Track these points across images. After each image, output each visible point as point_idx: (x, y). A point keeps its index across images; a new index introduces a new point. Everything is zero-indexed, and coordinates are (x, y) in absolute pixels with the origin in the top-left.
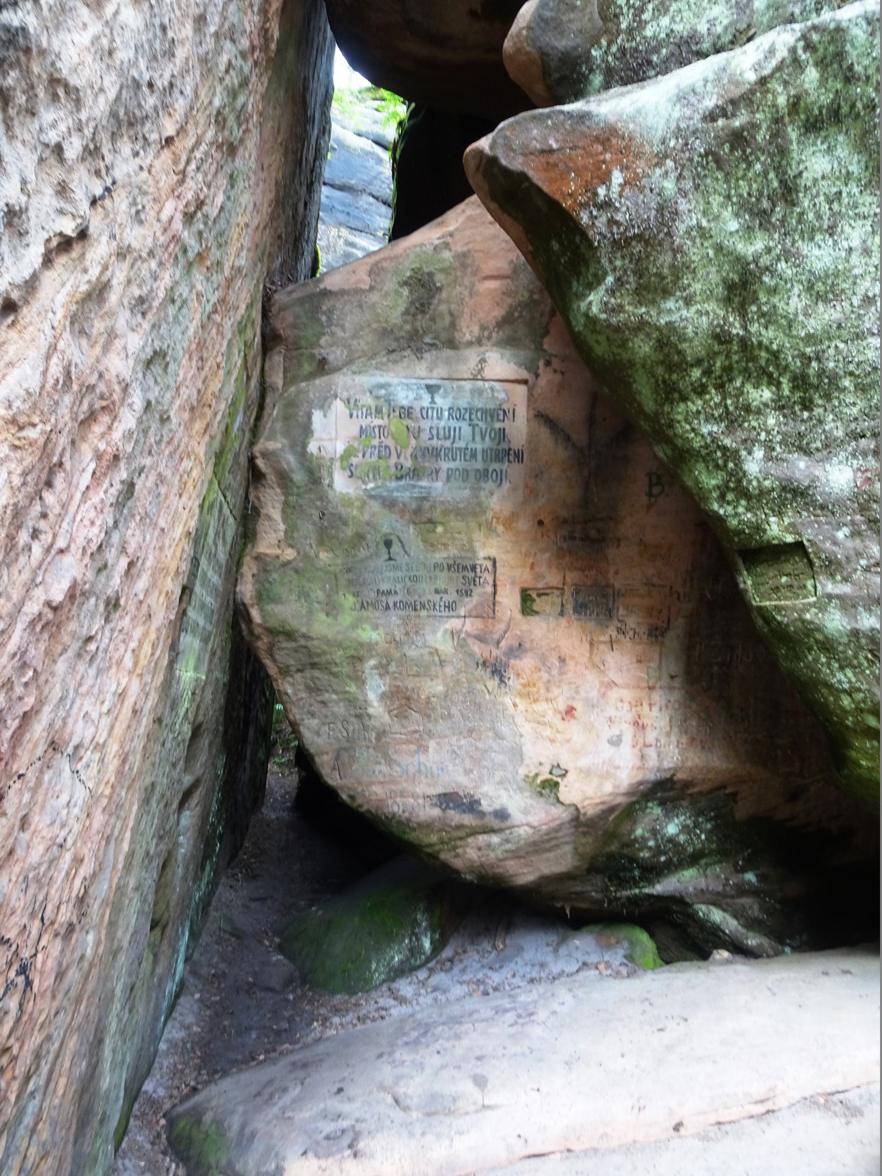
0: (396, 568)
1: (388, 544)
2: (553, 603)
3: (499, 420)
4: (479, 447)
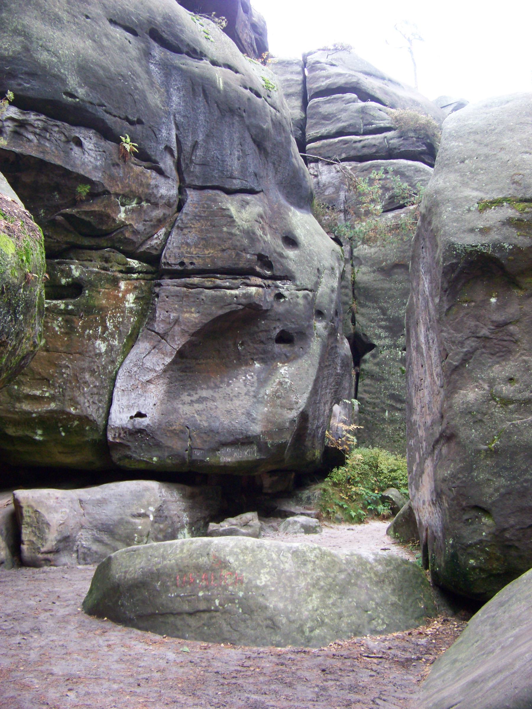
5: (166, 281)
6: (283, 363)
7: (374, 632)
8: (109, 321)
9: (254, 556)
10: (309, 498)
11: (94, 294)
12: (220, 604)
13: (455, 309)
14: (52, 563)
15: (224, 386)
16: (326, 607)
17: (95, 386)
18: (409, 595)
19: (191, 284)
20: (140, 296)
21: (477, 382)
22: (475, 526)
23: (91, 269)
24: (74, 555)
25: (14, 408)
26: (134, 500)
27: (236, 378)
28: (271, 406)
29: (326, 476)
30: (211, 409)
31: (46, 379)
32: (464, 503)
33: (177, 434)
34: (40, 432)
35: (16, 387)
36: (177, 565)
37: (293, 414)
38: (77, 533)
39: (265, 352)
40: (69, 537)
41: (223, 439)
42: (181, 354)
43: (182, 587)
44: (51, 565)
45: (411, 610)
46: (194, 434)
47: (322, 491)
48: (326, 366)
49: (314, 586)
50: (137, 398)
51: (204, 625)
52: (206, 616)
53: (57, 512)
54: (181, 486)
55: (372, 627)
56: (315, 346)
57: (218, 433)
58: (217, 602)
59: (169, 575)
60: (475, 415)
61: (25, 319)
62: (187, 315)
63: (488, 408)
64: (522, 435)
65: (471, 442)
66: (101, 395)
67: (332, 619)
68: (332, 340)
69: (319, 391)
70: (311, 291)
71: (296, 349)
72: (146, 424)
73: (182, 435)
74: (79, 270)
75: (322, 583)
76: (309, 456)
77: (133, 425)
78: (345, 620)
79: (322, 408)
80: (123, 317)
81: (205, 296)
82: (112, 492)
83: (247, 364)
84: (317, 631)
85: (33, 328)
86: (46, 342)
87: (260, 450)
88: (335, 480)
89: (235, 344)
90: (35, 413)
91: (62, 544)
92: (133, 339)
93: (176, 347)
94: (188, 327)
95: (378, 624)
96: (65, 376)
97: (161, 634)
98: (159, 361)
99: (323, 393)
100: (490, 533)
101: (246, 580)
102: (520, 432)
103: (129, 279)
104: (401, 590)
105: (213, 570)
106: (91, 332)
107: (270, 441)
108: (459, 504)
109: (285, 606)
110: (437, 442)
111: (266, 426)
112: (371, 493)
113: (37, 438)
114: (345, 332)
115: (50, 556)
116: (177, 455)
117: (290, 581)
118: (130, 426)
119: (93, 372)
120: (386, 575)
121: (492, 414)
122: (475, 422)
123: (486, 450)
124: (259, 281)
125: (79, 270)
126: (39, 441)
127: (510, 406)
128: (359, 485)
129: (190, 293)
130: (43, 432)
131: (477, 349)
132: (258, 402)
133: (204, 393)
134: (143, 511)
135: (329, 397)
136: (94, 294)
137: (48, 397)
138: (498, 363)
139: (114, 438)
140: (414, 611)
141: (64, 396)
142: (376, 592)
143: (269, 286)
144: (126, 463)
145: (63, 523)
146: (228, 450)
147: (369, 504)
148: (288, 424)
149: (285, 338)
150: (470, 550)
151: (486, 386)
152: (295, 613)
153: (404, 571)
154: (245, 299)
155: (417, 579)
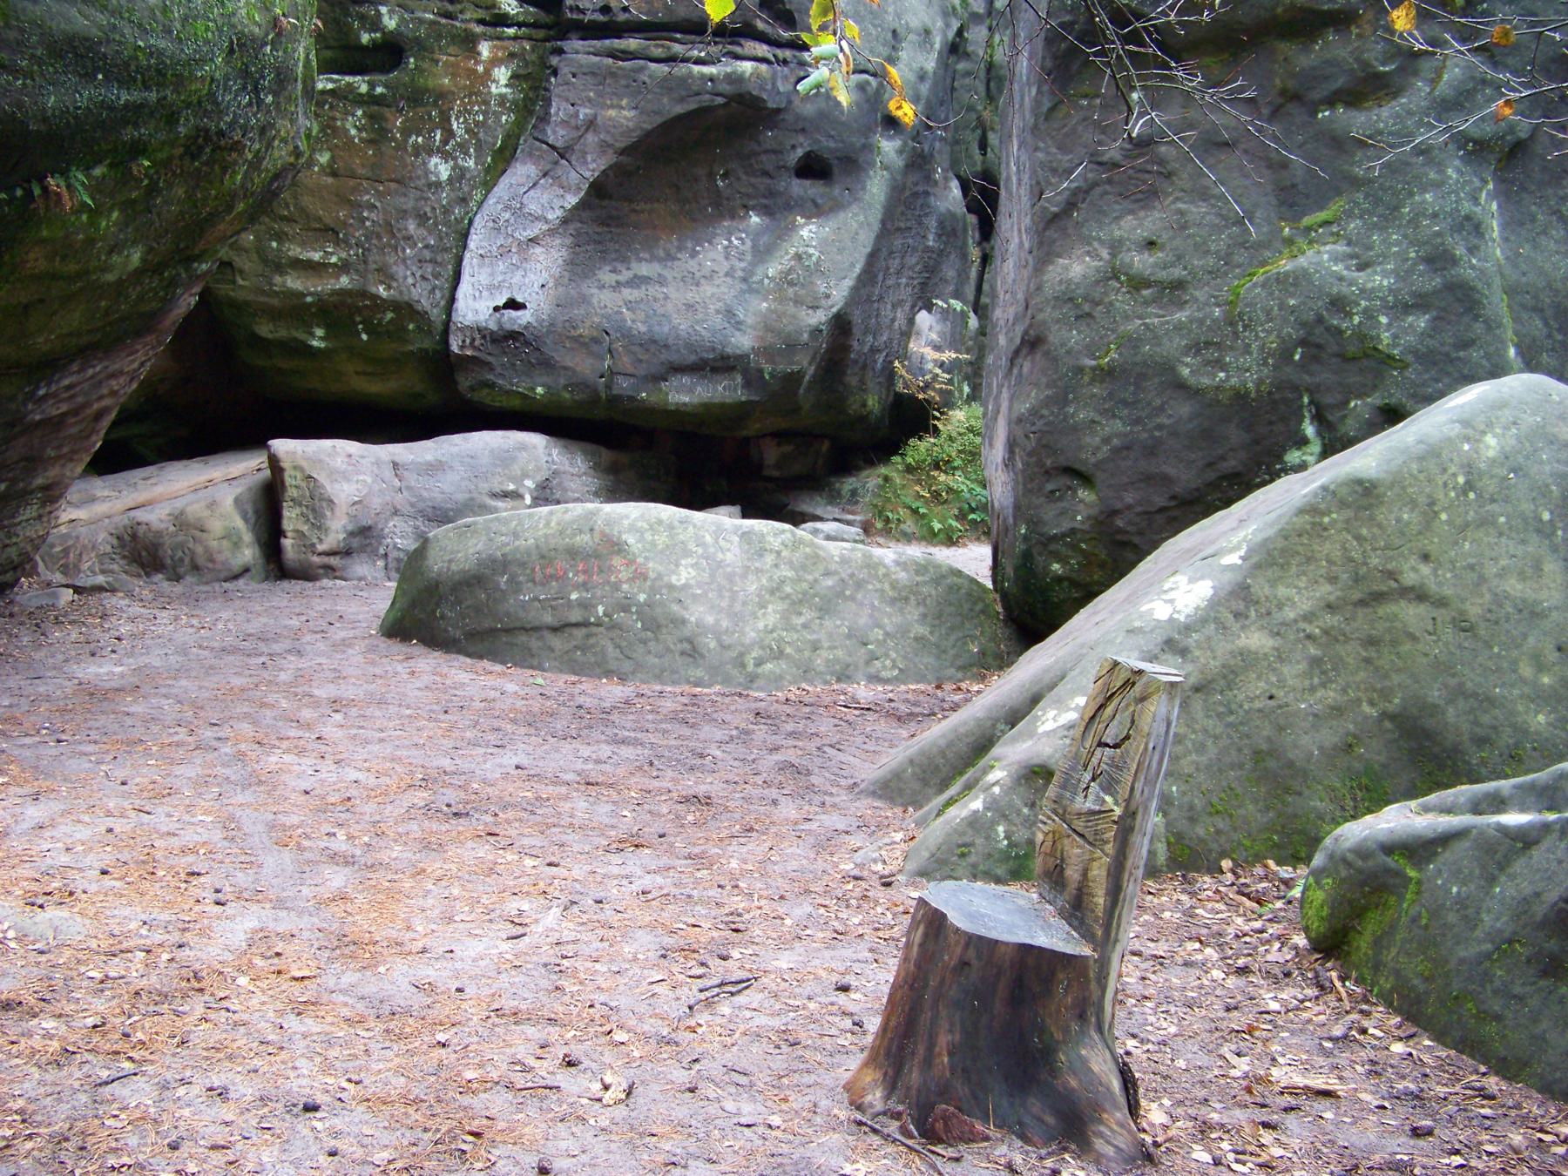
5: (574, 44)
6: (808, 218)
7: (875, 679)
8: (457, 119)
9: (671, 537)
10: (854, 493)
11: (425, 65)
12: (605, 614)
13: (1063, 109)
15: (683, 256)
16: (789, 628)
17: (426, 247)
18: (952, 629)
19: (623, 52)
20: (522, 72)
21: (1089, 244)
22: (1064, 504)
23: (419, 14)
24: (381, 563)
25: (271, 284)
26: (495, 465)
27: (710, 243)
28: (775, 300)
29: (895, 453)
30: (655, 300)
32: (1049, 462)
33: (584, 344)
34: (320, 332)
35: (274, 244)
36: (537, 547)
37: (819, 318)
38: (387, 521)
39: (771, 194)
40: (370, 528)
41: (675, 358)
42: (598, 190)
43: (543, 584)
45: (952, 652)
46: (618, 345)
47: (880, 481)
48: (899, 229)
49: (772, 592)
50: (508, 273)
51: (576, 647)
52: (579, 633)
53: (348, 481)
54: (590, 447)
55: (872, 670)
56: (876, 188)
57: (666, 346)
58: (601, 609)
59: (523, 565)
60: (1081, 306)
61: (277, 104)
62: (612, 113)
63: (1105, 293)
64: (1160, 345)
65: (1068, 352)
66: (440, 264)
67: (799, 650)
68: (912, 178)
69: (880, 277)
70: (874, 75)
71: (836, 192)
72: (523, 322)
73: (595, 348)
74: (396, 17)
75: (788, 589)
76: (853, 406)
77: (499, 323)
78: (824, 654)
79: (887, 311)
80: (485, 113)
81: (650, 77)
82: (455, 450)
83: (733, 217)
84: (769, 666)
85: (293, 122)
86: (333, 158)
87: (747, 384)
88: (909, 460)
89: (711, 176)
90: (311, 294)
92: (504, 157)
93: (588, 174)
94: (613, 136)
95: (884, 667)
97: (503, 663)
98: (553, 201)
99: (889, 283)
100: (1089, 518)
101: (652, 575)
102: (1156, 340)
103: (499, 38)
104: (939, 617)
105: (598, 556)
106: (420, 139)
107: (767, 368)
108: (1040, 464)
109: (717, 621)
110: (1017, 352)
111: (762, 338)
112: (978, 489)
113: (315, 343)
114: (954, 164)
115: (334, 561)
116: (583, 385)
117: (731, 582)
118: (493, 326)
119: (422, 219)
120: (914, 589)
121: (1111, 304)
122: (1077, 318)
123: (1093, 369)
124: (762, 50)
125: (396, 17)
126: (319, 349)
127: (1145, 292)
128: (958, 473)
129: (619, 68)
130: (327, 333)
131: (1096, 184)
132: (751, 291)
133: (644, 269)
134: (511, 487)
135: (906, 293)
136: (425, 65)
137: (335, 265)
138: (1132, 212)
139: (462, 347)
140: (957, 656)
142: (890, 616)
143: (785, 62)
144: (483, 396)
146: (686, 380)
147: (973, 510)
148: (806, 335)
149: (814, 168)
150: (1053, 547)
151: (1105, 254)
152: (733, 633)
153: (951, 588)
154: (729, 84)
155: (975, 603)
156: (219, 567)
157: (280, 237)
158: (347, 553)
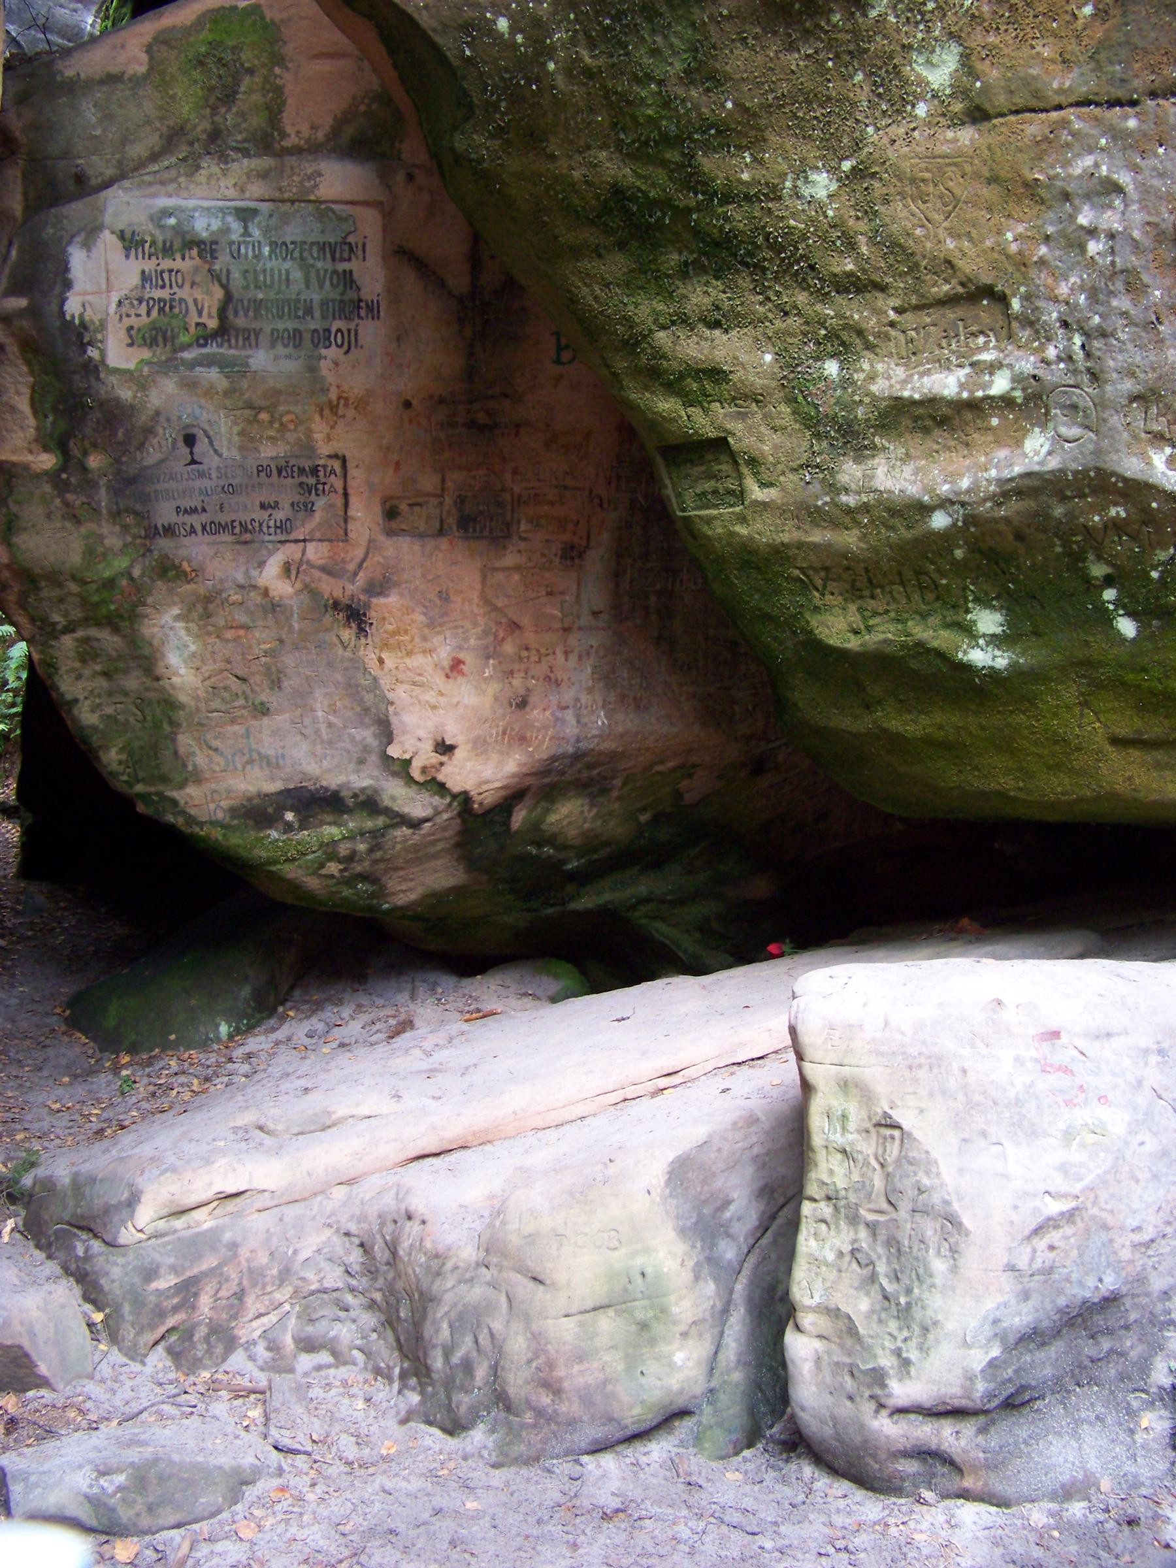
0: (201, 475)
1: (190, 440)
2: (429, 517)
3: (343, 260)
4: (316, 297)
14: (968, 1483)
25: (834, 489)
31: (988, 292)
34: (988, 621)
35: (832, 368)
40: (1111, 1301)
44: (965, 1495)
90: (945, 503)
91: (1056, 1349)
96: (1093, 247)
113: (979, 657)
115: (951, 1437)
130: (1011, 622)
137: (1006, 401)
141: (1095, 377)
145: (1070, 1216)
156: (569, 1408)
157: (843, 342)
158: (1014, 1402)
